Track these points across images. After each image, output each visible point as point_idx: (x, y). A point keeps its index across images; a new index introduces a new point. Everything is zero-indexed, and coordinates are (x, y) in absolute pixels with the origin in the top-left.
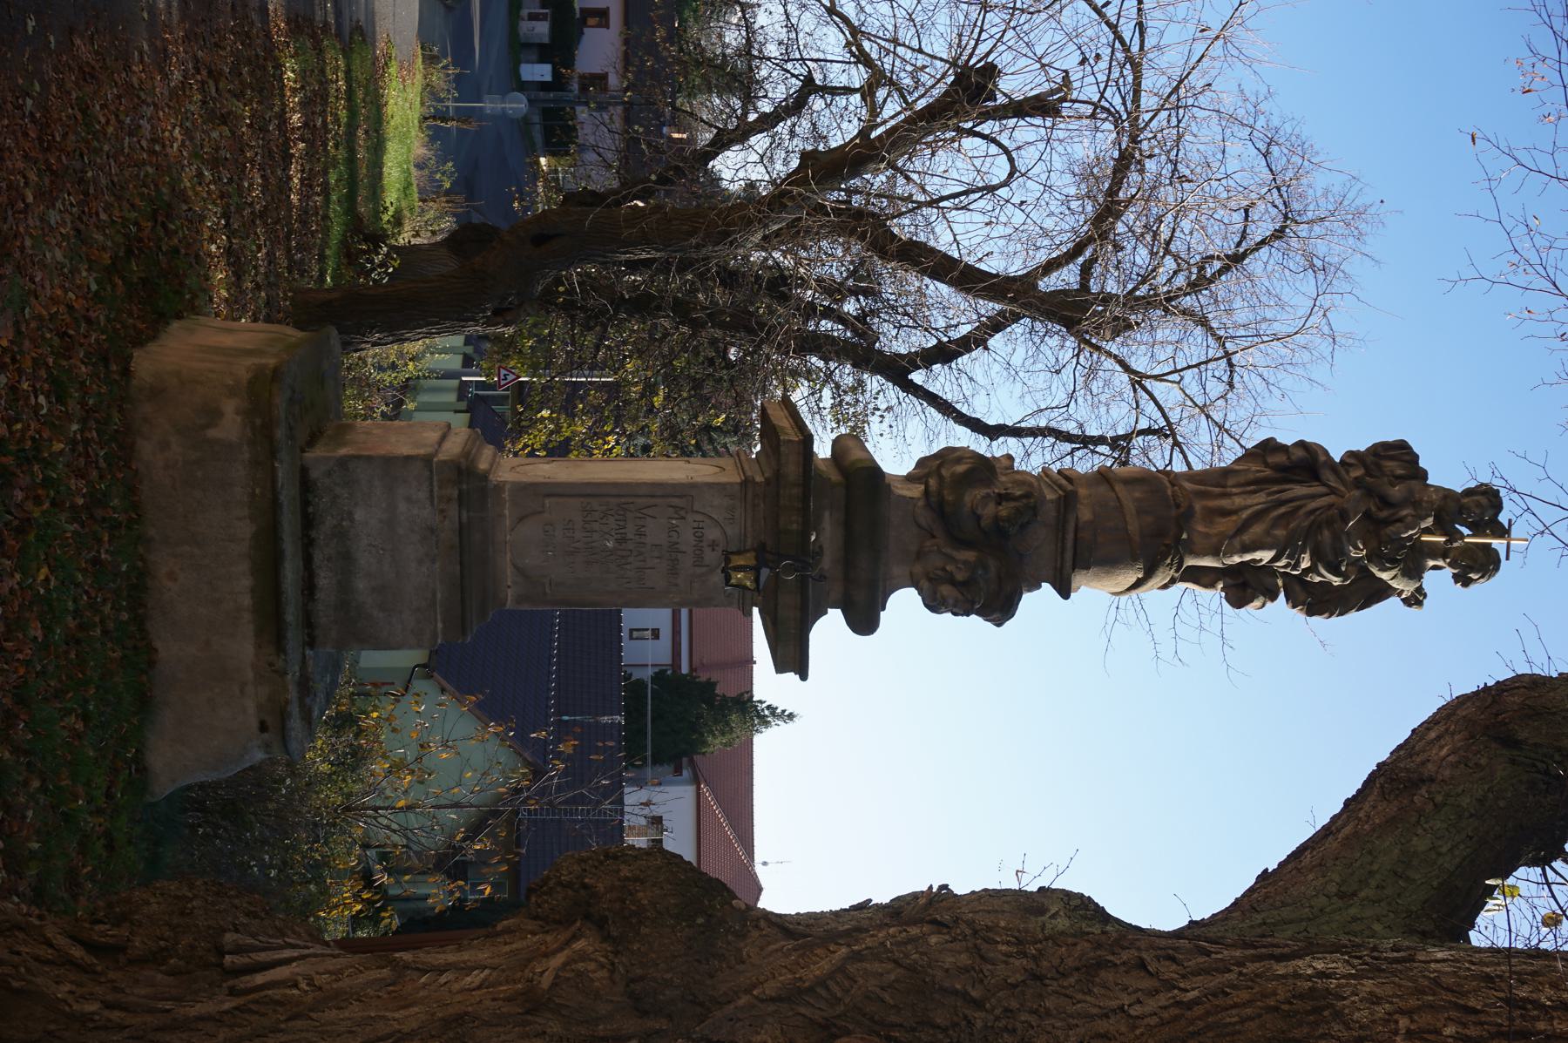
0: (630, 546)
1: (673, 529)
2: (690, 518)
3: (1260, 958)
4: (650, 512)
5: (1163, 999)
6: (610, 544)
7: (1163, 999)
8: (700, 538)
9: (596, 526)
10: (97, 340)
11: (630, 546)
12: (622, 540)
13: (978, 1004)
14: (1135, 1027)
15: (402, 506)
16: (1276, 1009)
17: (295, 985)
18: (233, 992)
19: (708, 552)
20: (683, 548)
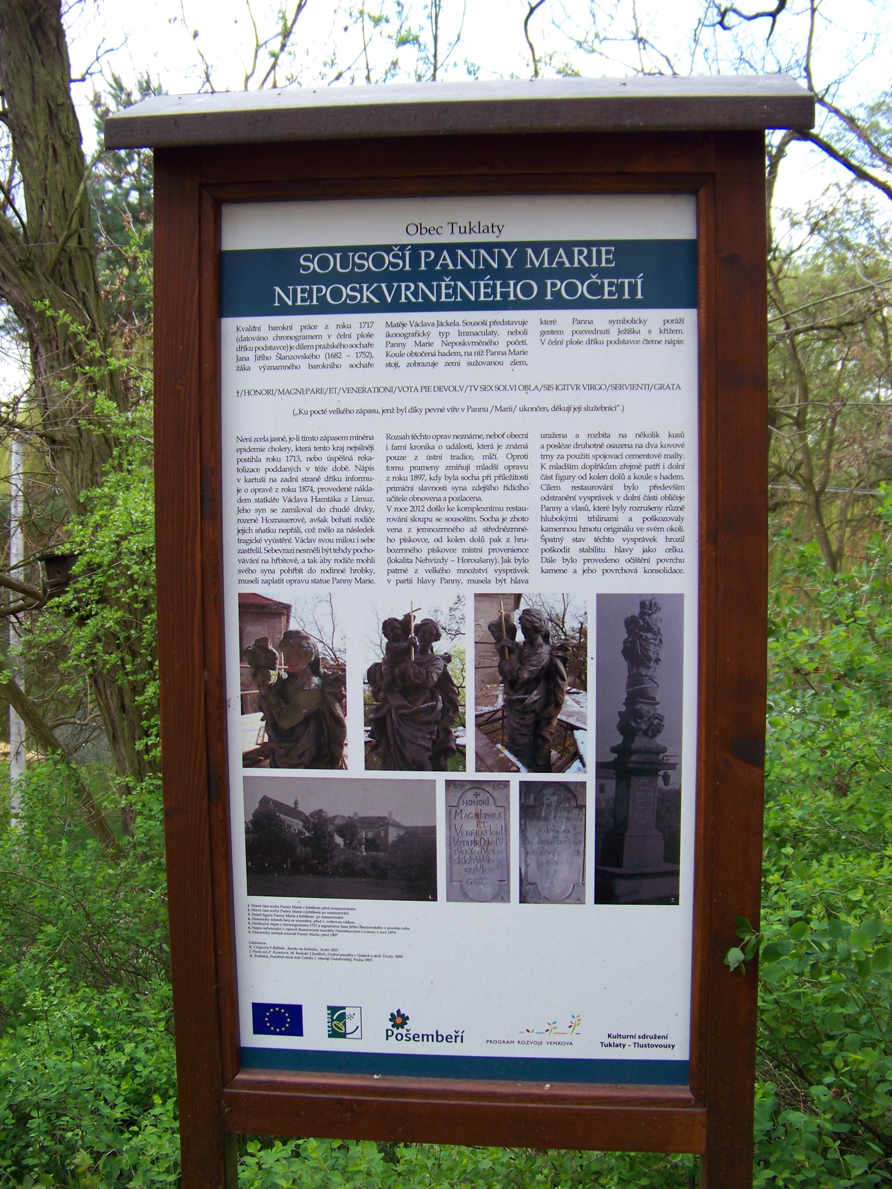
0: (478, 839)
2: (462, 807)
8: (473, 802)
9: (467, 857)
11: (478, 839)
12: (475, 843)
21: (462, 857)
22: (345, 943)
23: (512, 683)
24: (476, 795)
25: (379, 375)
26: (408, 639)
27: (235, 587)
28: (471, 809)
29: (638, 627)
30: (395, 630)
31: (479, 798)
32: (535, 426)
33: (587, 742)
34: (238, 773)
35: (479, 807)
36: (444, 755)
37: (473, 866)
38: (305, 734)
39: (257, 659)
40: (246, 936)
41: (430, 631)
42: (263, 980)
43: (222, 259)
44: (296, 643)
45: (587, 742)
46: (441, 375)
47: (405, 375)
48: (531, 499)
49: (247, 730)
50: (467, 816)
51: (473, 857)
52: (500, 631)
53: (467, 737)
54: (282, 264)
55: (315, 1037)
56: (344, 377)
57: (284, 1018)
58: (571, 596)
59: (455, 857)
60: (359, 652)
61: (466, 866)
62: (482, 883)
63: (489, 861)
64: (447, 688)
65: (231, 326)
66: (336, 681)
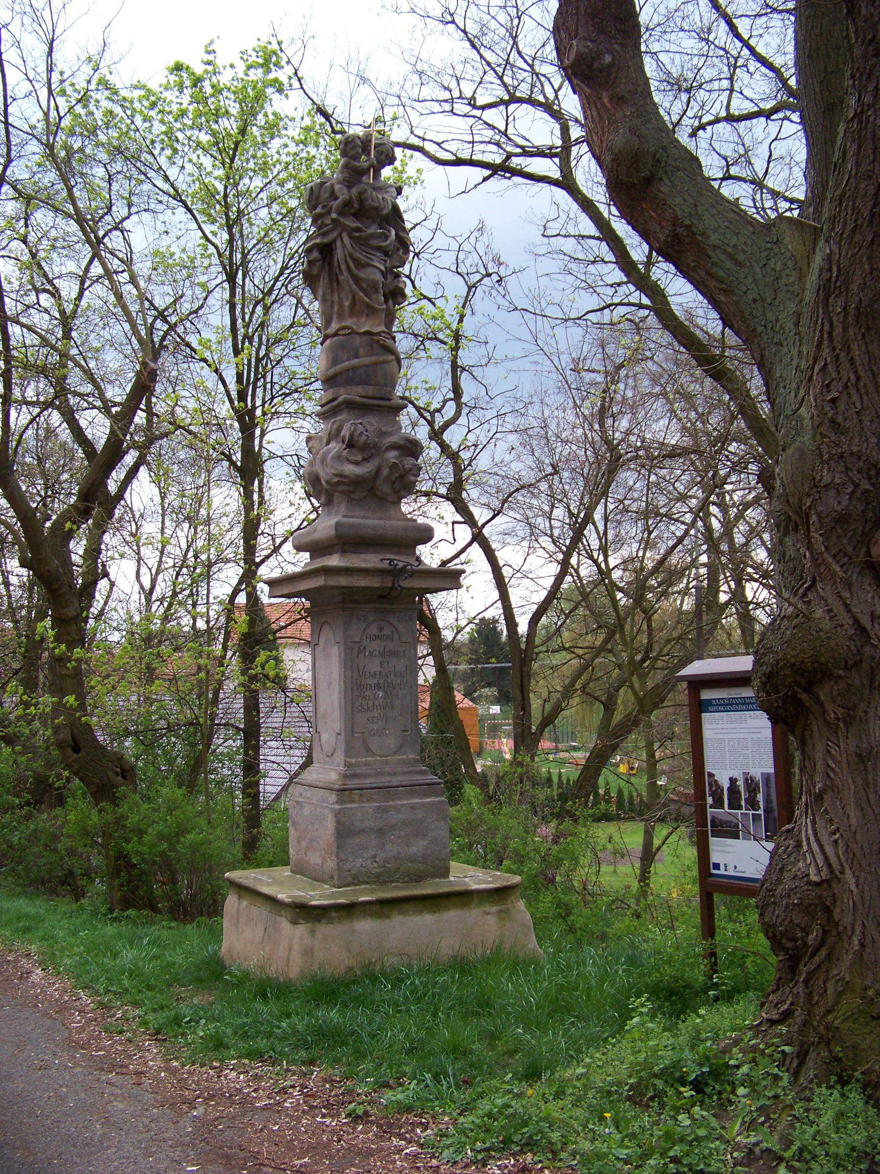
0: (381, 681)
1: (371, 654)
2: (365, 643)
3: (831, 339)
4: (361, 668)
5: (853, 392)
6: (381, 694)
7: (853, 392)
8: (376, 637)
9: (370, 703)
10: (445, 987)
11: (381, 681)
12: (378, 686)
13: (857, 486)
14: (868, 407)
15: (367, 824)
16: (863, 335)
17: (836, 841)
18: (842, 873)
19: (384, 632)
20: (382, 649)
21: (364, 703)
22: (727, 849)
23: (749, 792)
24: (380, 629)
25: (725, 726)
26: (733, 781)
27: (706, 771)
28: (376, 645)
29: (766, 777)
30: (731, 779)
31: (384, 632)
32: (750, 736)
33: (761, 804)
34: (709, 810)
35: (384, 643)
36: (739, 807)
37: (376, 714)
38: (718, 803)
39: (710, 785)
40: (711, 847)
41: (736, 780)
42: (715, 858)
43: (700, 702)
44: (716, 781)
45: (761, 804)
46: (734, 726)
47: (729, 726)
48: (749, 752)
49: (710, 800)
50: (371, 654)
51: (377, 703)
52: (746, 780)
53: (743, 803)
54: (709, 702)
55: (722, 872)
56: (720, 726)
57: (717, 866)
58: (757, 773)
59: (358, 704)
60: (726, 785)
61: (369, 714)
62: (748, 835)
63: (392, 708)
64: (739, 792)
65: (703, 715)
66: (722, 790)
